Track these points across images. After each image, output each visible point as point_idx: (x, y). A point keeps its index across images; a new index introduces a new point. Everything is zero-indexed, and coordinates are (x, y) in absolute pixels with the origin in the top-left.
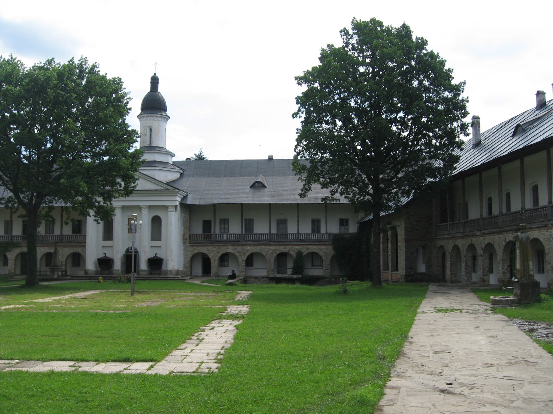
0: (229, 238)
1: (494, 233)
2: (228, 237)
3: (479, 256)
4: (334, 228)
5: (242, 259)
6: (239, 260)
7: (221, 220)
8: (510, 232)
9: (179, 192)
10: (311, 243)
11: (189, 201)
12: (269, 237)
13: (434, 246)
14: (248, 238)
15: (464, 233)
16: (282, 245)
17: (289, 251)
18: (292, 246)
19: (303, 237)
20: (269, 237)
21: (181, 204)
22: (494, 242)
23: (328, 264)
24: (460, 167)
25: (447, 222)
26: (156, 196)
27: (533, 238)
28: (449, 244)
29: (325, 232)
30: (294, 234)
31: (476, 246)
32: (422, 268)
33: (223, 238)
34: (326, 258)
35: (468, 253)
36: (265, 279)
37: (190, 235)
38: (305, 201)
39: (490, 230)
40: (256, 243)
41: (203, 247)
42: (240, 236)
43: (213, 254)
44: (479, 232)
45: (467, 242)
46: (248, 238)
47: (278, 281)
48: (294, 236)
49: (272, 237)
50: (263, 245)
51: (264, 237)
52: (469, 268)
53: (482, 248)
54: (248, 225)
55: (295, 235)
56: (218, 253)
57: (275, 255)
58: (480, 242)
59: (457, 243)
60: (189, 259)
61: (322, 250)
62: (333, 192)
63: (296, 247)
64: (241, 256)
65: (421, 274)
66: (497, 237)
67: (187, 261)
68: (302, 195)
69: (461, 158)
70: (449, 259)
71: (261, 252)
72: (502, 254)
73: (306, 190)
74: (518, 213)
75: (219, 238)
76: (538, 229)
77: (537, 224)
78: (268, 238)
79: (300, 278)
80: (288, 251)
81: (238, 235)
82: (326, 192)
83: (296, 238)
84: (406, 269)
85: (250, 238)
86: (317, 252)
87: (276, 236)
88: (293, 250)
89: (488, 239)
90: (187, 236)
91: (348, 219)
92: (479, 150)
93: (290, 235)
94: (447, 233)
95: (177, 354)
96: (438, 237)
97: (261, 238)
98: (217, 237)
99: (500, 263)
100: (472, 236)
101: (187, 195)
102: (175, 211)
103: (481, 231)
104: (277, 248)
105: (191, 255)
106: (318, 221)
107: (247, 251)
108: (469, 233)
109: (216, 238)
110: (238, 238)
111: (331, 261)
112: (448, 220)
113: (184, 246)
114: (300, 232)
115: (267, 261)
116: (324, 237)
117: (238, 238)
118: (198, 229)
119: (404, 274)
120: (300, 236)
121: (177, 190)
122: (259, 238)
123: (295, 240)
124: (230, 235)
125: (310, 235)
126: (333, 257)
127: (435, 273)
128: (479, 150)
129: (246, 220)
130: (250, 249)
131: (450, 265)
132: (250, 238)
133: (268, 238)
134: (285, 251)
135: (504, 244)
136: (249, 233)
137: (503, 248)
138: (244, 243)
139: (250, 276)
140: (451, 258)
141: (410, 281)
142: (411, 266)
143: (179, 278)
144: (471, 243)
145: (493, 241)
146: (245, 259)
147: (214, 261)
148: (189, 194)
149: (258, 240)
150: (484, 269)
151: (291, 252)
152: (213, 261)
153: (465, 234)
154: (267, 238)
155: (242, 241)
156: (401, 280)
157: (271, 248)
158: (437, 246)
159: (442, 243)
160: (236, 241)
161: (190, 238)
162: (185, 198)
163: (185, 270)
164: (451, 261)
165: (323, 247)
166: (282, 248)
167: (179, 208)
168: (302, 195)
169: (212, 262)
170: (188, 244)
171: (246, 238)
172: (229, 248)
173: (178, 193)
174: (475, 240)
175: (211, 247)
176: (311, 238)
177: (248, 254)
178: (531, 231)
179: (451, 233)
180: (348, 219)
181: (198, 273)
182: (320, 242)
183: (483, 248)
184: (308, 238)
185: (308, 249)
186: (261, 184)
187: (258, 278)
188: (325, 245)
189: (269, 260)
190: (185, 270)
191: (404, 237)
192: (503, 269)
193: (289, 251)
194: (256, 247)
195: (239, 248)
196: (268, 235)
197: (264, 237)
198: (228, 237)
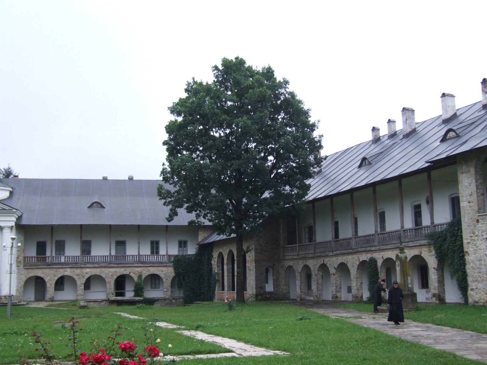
0: (67, 260)
1: (348, 254)
2: (66, 259)
3: (331, 274)
4: (174, 251)
5: (81, 282)
6: (78, 283)
7: (56, 241)
8: (364, 253)
9: (17, 212)
10: (151, 265)
11: (24, 222)
12: (109, 259)
13: (282, 266)
14: (87, 260)
15: (315, 254)
16: (122, 267)
17: (130, 273)
18: (133, 268)
19: (143, 259)
20: (109, 259)
21: (16, 224)
22: (347, 261)
23: (168, 286)
24: (311, 196)
25: (296, 244)
26: (6, 216)
27: (386, 258)
28: (298, 264)
29: (165, 253)
30: (134, 256)
31: (328, 265)
32: (269, 288)
33: (60, 260)
34: (167, 279)
35: (319, 272)
36: (105, 302)
37: (25, 257)
38: (174, 223)
39: (343, 251)
40: (96, 265)
41: (39, 270)
42: (79, 258)
43: (49, 278)
44: (331, 253)
45: (320, 262)
46: (87, 260)
47: (120, 303)
48: (134, 258)
49: (141, 259)
50: (103, 267)
51: (104, 259)
52: (320, 286)
53: (334, 267)
54: (86, 248)
55: (135, 257)
56: (55, 276)
57: (115, 277)
58: (333, 262)
59: (307, 264)
60: (23, 283)
61: (162, 271)
62: (198, 216)
63: (137, 269)
64: (80, 279)
65: (270, 293)
66: (350, 257)
67: (20, 285)
68: (170, 219)
69: (311, 189)
70: (299, 279)
71: (101, 275)
72: (355, 273)
73: (173, 214)
74: (371, 236)
75: (56, 260)
76: (391, 250)
77: (390, 245)
78: (108, 260)
79: (142, 300)
80: (128, 274)
81: (105, 256)
82: (192, 216)
83: (136, 259)
84: (256, 288)
85: (90, 260)
86: (157, 274)
87: (114, 258)
88: (134, 272)
89: (341, 259)
90: (21, 258)
91: (187, 240)
92: (325, 183)
93: (131, 257)
94: (296, 254)
95: (245, 354)
96: (286, 258)
97: (101, 260)
98: (55, 259)
99: (353, 281)
100: (324, 256)
101: (21, 216)
102: (11, 233)
103: (333, 252)
104: (118, 270)
105: (25, 279)
106: (157, 243)
107: (87, 273)
108: (321, 254)
109: (53, 260)
110: (76, 260)
111: (171, 282)
112: (298, 242)
113: (17, 269)
114: (141, 254)
115: (107, 284)
116: (165, 259)
117: (76, 260)
118: (32, 252)
119: (255, 293)
120: (141, 257)
121: (14, 210)
122: (99, 260)
123: (136, 262)
124: (161, 256)
125: (149, 256)
126: (174, 278)
127: (283, 291)
128: (325, 183)
129: (56, 241)
130: (89, 272)
131: (299, 284)
132: (90, 260)
133: (108, 260)
134: (125, 273)
135: (358, 263)
136: (88, 255)
137: (357, 267)
138: (82, 266)
139: (90, 300)
140: (300, 277)
141: (260, 300)
142: (260, 287)
143: (16, 303)
144: (323, 263)
145: (346, 261)
146: (84, 282)
147: (51, 285)
148: (23, 214)
149: (97, 262)
150: (336, 286)
151: (132, 274)
152: (49, 285)
153: (316, 254)
154: (107, 261)
155: (81, 263)
156: (250, 299)
157: (111, 270)
158: (285, 267)
159: (291, 263)
160: (74, 264)
161: (25, 261)
162: (19, 218)
163: (18, 294)
164: (301, 280)
165: (164, 269)
166: (122, 270)
167: (14, 228)
168: (170, 219)
169: (48, 285)
170: (22, 267)
171: (85, 260)
172: (67, 271)
173: (15, 213)
174: (327, 261)
175: (47, 270)
176: (152, 259)
177: (87, 276)
178: (384, 252)
179: (300, 254)
180: (187, 240)
181: (30, 298)
182: (160, 264)
183: (336, 267)
184: (149, 260)
185: (149, 271)
186: (99, 205)
187: (97, 301)
188: (166, 266)
189: (109, 282)
190: (18, 294)
191: (254, 258)
192: (357, 285)
193: (130, 273)
194: (95, 270)
195: (78, 271)
196: (108, 256)
197: (104, 259)
198: (66, 259)
